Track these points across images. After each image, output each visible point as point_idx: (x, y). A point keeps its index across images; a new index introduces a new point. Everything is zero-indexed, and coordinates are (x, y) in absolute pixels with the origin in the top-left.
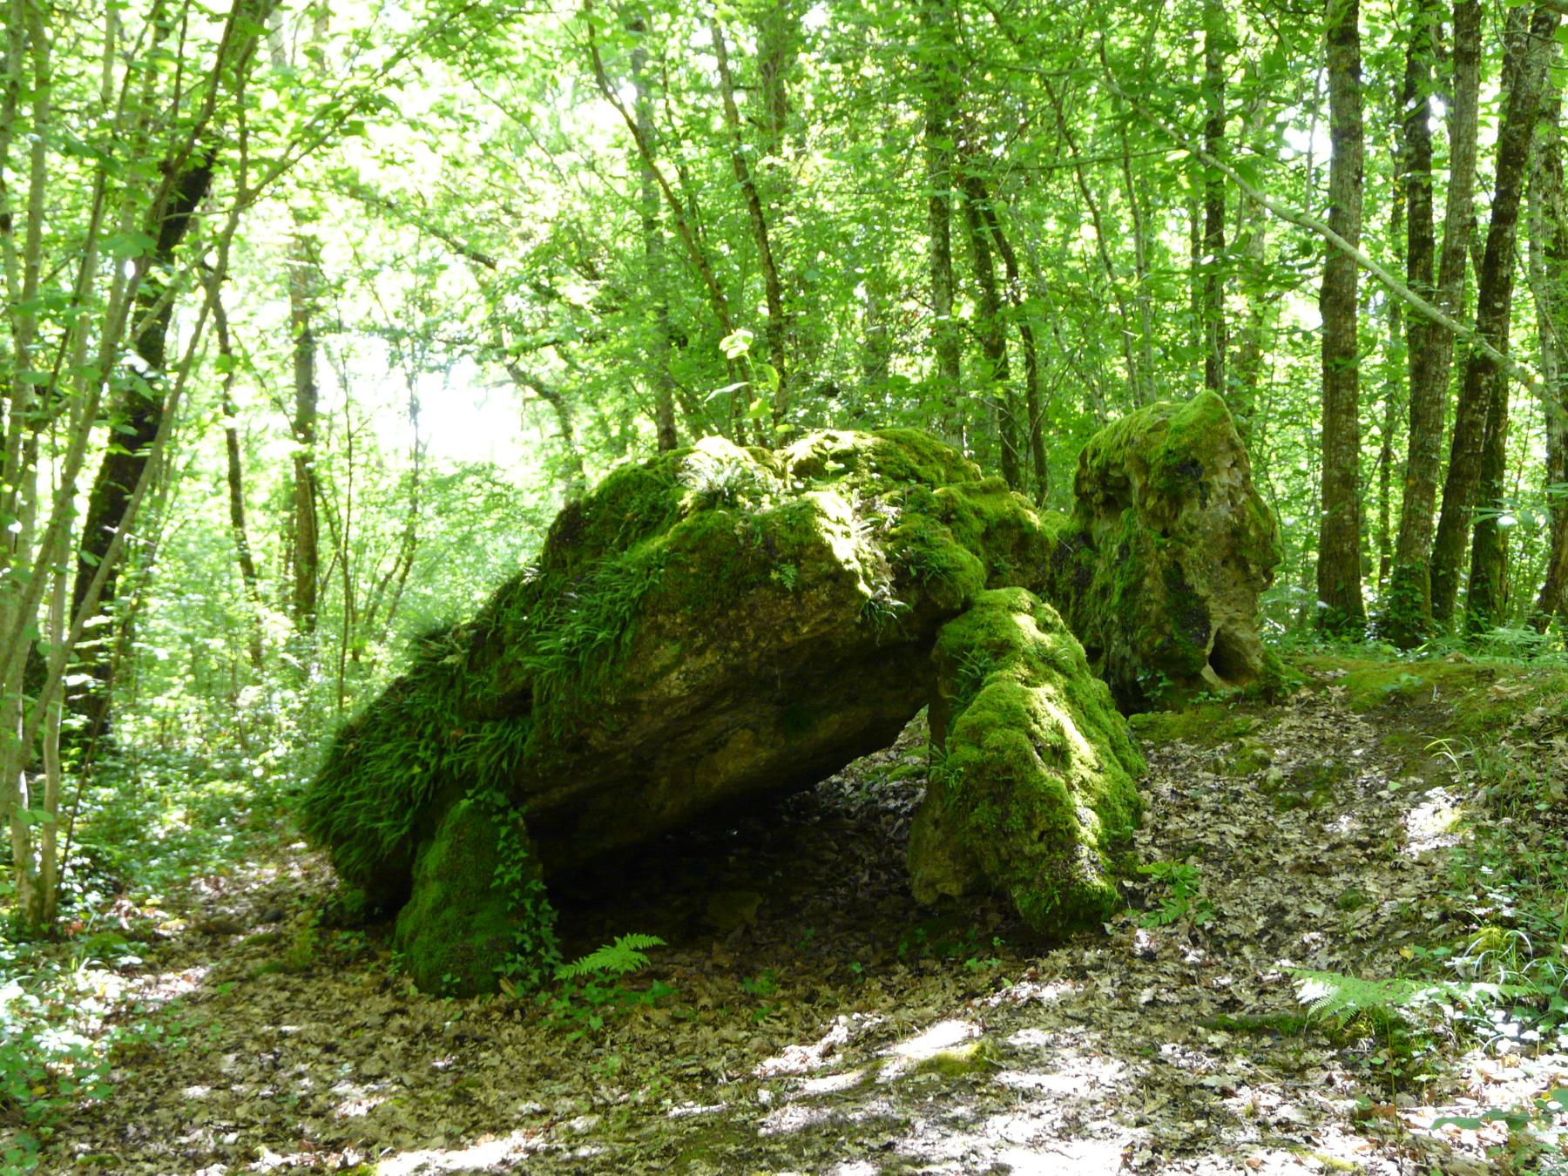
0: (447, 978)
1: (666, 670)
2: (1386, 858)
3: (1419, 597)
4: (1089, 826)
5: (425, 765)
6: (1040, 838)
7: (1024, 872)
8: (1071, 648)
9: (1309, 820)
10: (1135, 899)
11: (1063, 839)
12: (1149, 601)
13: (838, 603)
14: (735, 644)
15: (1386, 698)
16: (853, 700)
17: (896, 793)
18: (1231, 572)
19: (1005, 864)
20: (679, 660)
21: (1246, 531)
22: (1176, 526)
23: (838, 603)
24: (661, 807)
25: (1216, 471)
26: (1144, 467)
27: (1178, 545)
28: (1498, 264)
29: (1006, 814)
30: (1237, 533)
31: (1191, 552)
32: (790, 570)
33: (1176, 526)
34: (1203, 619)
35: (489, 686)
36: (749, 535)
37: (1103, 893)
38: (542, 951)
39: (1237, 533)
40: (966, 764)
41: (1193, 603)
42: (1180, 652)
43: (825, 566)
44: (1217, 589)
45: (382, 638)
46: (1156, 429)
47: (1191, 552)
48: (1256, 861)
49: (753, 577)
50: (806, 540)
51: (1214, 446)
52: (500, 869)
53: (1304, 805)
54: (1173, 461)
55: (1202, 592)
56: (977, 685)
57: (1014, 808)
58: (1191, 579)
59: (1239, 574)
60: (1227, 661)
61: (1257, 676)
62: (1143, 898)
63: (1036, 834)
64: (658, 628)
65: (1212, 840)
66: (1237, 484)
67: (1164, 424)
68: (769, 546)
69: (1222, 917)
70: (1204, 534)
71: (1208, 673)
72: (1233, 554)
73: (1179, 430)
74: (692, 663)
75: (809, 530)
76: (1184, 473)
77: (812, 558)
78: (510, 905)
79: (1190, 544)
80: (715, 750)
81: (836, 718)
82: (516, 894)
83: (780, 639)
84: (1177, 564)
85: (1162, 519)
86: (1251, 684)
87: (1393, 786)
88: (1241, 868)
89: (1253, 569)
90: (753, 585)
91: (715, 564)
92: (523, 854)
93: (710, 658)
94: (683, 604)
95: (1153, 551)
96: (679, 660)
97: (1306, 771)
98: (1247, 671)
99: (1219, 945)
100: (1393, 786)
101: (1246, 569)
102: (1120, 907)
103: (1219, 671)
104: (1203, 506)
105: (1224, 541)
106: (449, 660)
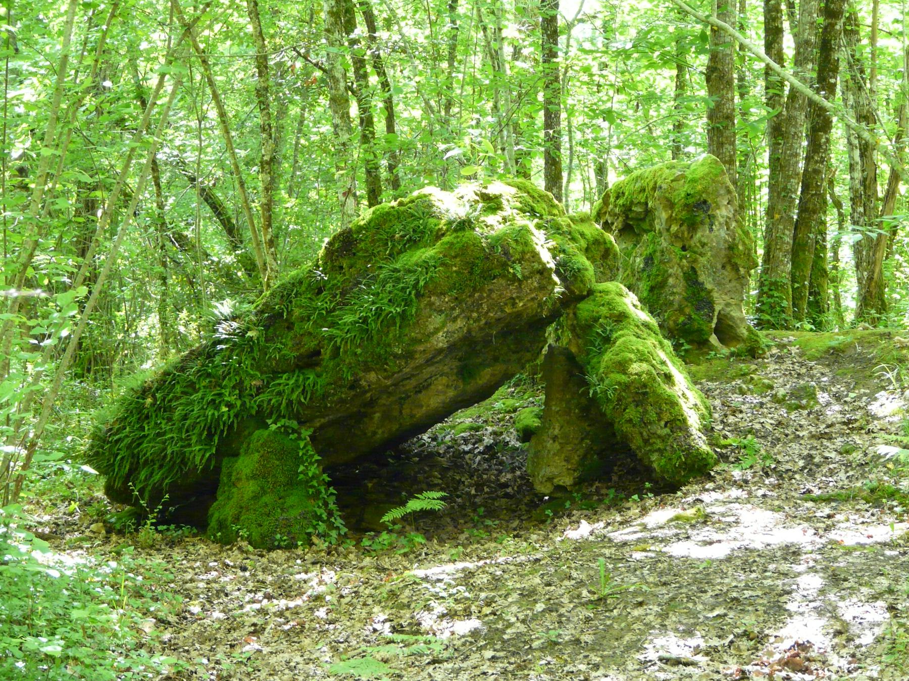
0: (278, 536)
1: (437, 330)
2: (862, 428)
3: (785, 304)
4: (694, 421)
5: (230, 405)
6: (666, 426)
7: (659, 445)
8: (653, 321)
9: (809, 414)
10: (724, 458)
11: (678, 424)
12: (673, 294)
13: (542, 288)
14: (475, 315)
15: (827, 352)
16: (496, 359)
17: (466, 441)
18: (728, 273)
19: (646, 442)
20: (444, 325)
21: (737, 245)
22: (692, 243)
23: (542, 288)
24: (374, 433)
25: (718, 207)
26: (670, 205)
27: (694, 256)
28: (831, 49)
29: (646, 412)
30: (731, 248)
31: (703, 260)
32: (518, 267)
33: (692, 243)
34: (710, 304)
35: (285, 348)
36: (492, 247)
37: (708, 454)
38: (333, 520)
39: (731, 248)
40: (619, 383)
41: (703, 294)
42: (696, 326)
43: (536, 265)
44: (719, 284)
46: (676, 180)
47: (703, 260)
48: (787, 435)
49: (496, 272)
50: (526, 249)
51: (717, 191)
52: (301, 468)
53: (804, 408)
54: (691, 201)
55: (709, 286)
56: (607, 340)
57: (650, 408)
58: (702, 278)
59: (732, 275)
60: (726, 331)
61: (744, 341)
62: (728, 457)
63: (663, 423)
64: (431, 304)
65: (758, 426)
66: (731, 216)
67: (683, 176)
68: (506, 253)
69: (779, 462)
70: (712, 248)
71: (713, 339)
72: (730, 261)
73: (694, 181)
74: (451, 327)
75: (526, 244)
76: (696, 210)
77: (528, 260)
78: (311, 491)
79: (702, 255)
80: (420, 392)
81: (488, 370)
82: (315, 483)
83: (502, 311)
84: (693, 269)
85: (682, 239)
86: (740, 346)
87: (852, 395)
88: (778, 440)
89: (742, 271)
90: (495, 277)
91: (471, 266)
92: (317, 457)
93: (460, 323)
94: (450, 289)
95: (677, 260)
96: (444, 325)
97: (798, 390)
98: (737, 338)
99: (781, 476)
100: (852, 395)
101: (738, 270)
102: (717, 462)
103: (721, 340)
104: (711, 230)
105: (723, 252)
106: (250, 334)
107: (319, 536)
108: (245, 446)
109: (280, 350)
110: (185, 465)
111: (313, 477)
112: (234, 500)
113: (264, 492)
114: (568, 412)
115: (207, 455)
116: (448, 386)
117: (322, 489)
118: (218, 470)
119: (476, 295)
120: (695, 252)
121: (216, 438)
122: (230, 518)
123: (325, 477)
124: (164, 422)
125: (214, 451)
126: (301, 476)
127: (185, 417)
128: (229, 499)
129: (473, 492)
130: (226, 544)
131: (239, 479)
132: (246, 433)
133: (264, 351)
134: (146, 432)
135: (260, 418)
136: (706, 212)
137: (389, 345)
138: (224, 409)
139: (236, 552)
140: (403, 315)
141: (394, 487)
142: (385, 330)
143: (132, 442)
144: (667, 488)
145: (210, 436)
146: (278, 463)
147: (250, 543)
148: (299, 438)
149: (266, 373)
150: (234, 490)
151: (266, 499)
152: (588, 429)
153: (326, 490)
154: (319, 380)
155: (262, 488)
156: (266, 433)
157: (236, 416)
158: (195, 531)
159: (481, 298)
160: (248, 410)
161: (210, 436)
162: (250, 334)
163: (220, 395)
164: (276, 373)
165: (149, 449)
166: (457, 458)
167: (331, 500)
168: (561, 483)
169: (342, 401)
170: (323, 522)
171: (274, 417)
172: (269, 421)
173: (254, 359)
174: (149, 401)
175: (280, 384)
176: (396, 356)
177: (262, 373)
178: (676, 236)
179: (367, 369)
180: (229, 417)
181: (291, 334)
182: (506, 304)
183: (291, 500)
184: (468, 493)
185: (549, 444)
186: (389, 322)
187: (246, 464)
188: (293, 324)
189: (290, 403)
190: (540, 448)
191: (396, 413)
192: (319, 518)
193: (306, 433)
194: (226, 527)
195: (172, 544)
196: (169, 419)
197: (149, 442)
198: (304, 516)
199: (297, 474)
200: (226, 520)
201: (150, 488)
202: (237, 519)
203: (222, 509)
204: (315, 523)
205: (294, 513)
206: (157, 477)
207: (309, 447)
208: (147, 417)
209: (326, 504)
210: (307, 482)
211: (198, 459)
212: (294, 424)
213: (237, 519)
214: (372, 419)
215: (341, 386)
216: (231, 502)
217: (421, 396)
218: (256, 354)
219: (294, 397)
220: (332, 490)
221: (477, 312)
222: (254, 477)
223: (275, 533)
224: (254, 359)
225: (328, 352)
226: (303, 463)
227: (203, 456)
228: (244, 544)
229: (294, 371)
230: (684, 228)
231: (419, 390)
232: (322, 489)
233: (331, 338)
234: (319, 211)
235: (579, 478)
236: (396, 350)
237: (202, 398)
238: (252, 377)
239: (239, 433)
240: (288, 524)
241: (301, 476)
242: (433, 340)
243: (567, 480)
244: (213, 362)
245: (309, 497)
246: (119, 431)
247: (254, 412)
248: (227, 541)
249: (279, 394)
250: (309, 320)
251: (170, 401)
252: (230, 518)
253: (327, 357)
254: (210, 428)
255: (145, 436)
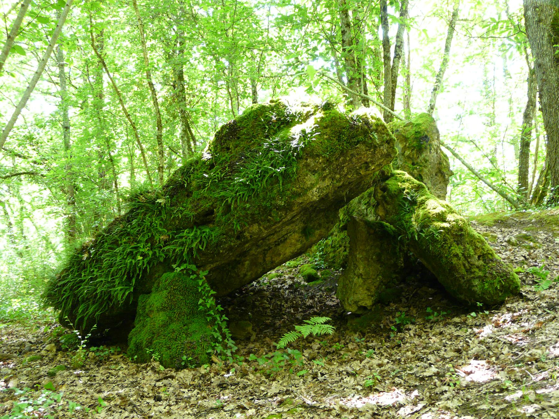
0: (184, 358)
1: (313, 185)
5: (144, 255)
17: (277, 283)
18: (439, 178)
22: (419, 161)
24: (245, 275)
31: (426, 170)
33: (419, 161)
35: (187, 209)
40: (443, 228)
45: (336, 43)
47: (426, 170)
51: (432, 131)
52: (201, 301)
57: (468, 246)
64: (307, 165)
78: (209, 319)
80: (279, 244)
82: (212, 312)
92: (212, 292)
93: (327, 182)
101: (444, 177)
104: (430, 153)
106: (158, 201)
107: (217, 355)
108: (155, 285)
109: (182, 212)
110: (111, 301)
111: (210, 308)
112: (148, 327)
113: (171, 320)
114: (367, 259)
115: (127, 293)
116: (297, 241)
117: (218, 317)
118: (135, 303)
119: (342, 158)
120: (421, 166)
121: (134, 281)
122: (145, 343)
123: (219, 307)
124: (96, 270)
125: (132, 290)
126: (201, 307)
127: (111, 266)
128: (144, 326)
129: (292, 311)
130: (142, 362)
131: (151, 311)
132: (157, 275)
133: (169, 213)
134: (83, 278)
135: (167, 265)
136: (427, 142)
137: (274, 199)
138: (139, 258)
139: (150, 372)
140: (284, 175)
141: (242, 310)
142: (270, 187)
143: (73, 286)
144: (493, 305)
145: (129, 279)
146: (181, 297)
147: (161, 363)
148: (198, 278)
149: (171, 230)
150: (148, 319)
151: (173, 326)
152: (380, 268)
153: (221, 317)
154: (213, 233)
155: (170, 318)
156: (172, 275)
157: (149, 263)
158: (119, 349)
159: (344, 161)
160: (158, 258)
161: (129, 279)
162: (158, 201)
163: (136, 248)
164: (178, 230)
165: (85, 290)
166: (276, 293)
167: (224, 325)
168: (363, 305)
169: (231, 249)
170: (219, 343)
171: (178, 263)
172: (174, 266)
173: (162, 220)
174: (85, 256)
175: (182, 237)
176: (279, 208)
177: (168, 230)
178: (409, 157)
179: (254, 221)
180: (143, 264)
181: (190, 199)
182: (361, 168)
183: (193, 327)
184: (289, 312)
185: (356, 279)
186: (274, 179)
187: (156, 299)
188: (191, 193)
189: (191, 250)
190: (347, 282)
191: (261, 261)
192: (216, 341)
193: (203, 274)
194: (142, 349)
195: (99, 363)
196: (100, 268)
197: (86, 285)
198: (204, 339)
199: (198, 306)
200: (141, 343)
201: (86, 318)
202: (150, 343)
203: (139, 335)
204: (213, 344)
205: (196, 337)
206: (91, 310)
207: (206, 285)
208: (84, 267)
209: (220, 329)
210: (205, 312)
211: (120, 296)
212: (193, 267)
213: (150, 343)
214: (243, 265)
215: (231, 237)
216: (145, 329)
217: (279, 247)
218: (164, 216)
219: (194, 245)
220: (224, 317)
221: (339, 174)
222: (163, 309)
223: (182, 354)
224: (162, 220)
225: (221, 209)
226: (201, 296)
227: (124, 294)
228: (156, 364)
229: (193, 228)
230: (414, 152)
231: (277, 244)
232: (218, 317)
233: (223, 198)
234: (215, 110)
235: (375, 301)
236: (279, 202)
237: (123, 251)
238: (161, 233)
239: (152, 274)
240: (192, 347)
241: (201, 307)
242: (309, 194)
243: (368, 303)
244: (131, 224)
245: (207, 323)
246: (64, 278)
247: (162, 260)
248: (142, 360)
249: (182, 244)
250: (204, 187)
251: (101, 255)
252: (145, 343)
253: (219, 214)
254: (129, 273)
255: (82, 281)
